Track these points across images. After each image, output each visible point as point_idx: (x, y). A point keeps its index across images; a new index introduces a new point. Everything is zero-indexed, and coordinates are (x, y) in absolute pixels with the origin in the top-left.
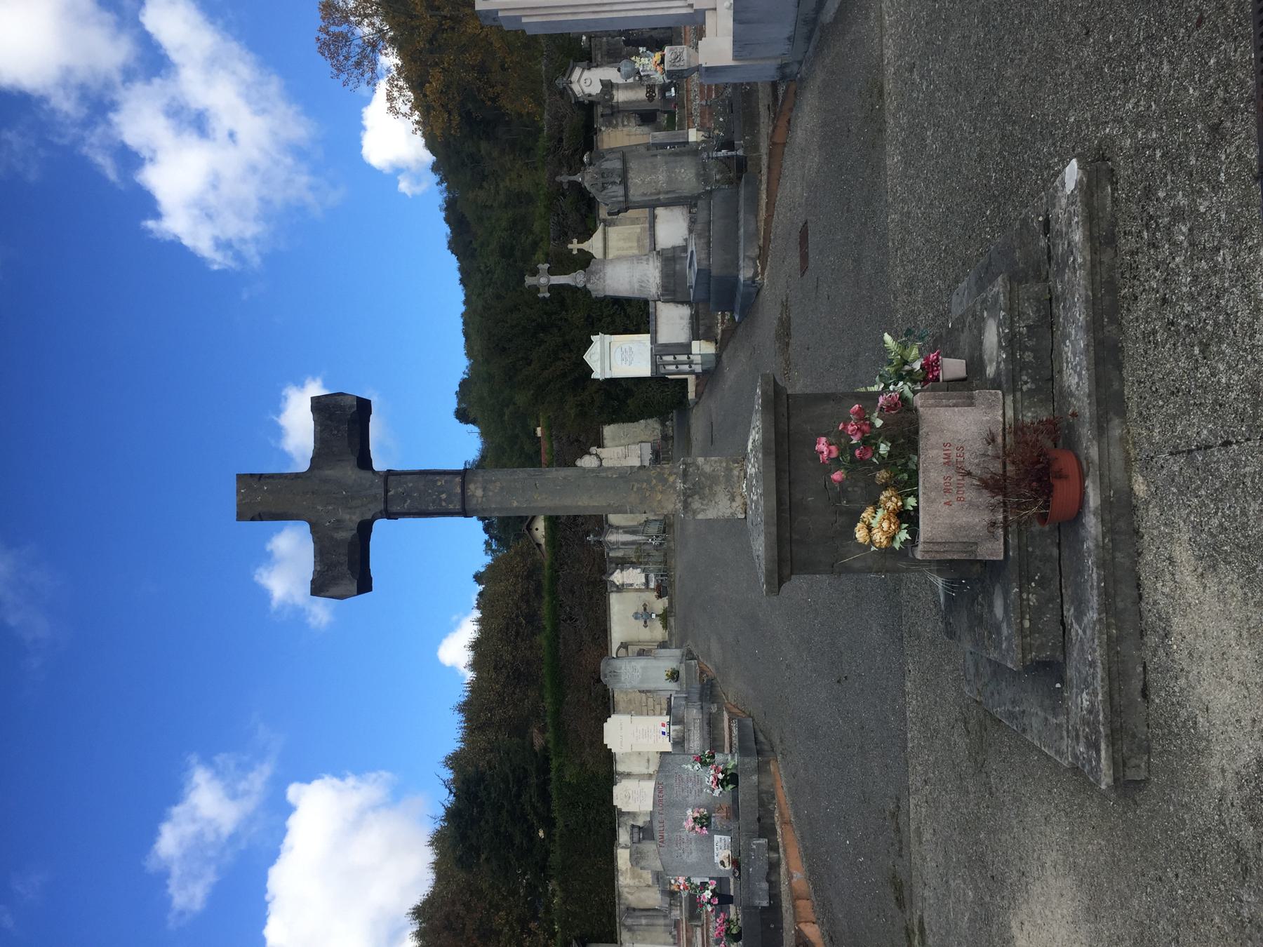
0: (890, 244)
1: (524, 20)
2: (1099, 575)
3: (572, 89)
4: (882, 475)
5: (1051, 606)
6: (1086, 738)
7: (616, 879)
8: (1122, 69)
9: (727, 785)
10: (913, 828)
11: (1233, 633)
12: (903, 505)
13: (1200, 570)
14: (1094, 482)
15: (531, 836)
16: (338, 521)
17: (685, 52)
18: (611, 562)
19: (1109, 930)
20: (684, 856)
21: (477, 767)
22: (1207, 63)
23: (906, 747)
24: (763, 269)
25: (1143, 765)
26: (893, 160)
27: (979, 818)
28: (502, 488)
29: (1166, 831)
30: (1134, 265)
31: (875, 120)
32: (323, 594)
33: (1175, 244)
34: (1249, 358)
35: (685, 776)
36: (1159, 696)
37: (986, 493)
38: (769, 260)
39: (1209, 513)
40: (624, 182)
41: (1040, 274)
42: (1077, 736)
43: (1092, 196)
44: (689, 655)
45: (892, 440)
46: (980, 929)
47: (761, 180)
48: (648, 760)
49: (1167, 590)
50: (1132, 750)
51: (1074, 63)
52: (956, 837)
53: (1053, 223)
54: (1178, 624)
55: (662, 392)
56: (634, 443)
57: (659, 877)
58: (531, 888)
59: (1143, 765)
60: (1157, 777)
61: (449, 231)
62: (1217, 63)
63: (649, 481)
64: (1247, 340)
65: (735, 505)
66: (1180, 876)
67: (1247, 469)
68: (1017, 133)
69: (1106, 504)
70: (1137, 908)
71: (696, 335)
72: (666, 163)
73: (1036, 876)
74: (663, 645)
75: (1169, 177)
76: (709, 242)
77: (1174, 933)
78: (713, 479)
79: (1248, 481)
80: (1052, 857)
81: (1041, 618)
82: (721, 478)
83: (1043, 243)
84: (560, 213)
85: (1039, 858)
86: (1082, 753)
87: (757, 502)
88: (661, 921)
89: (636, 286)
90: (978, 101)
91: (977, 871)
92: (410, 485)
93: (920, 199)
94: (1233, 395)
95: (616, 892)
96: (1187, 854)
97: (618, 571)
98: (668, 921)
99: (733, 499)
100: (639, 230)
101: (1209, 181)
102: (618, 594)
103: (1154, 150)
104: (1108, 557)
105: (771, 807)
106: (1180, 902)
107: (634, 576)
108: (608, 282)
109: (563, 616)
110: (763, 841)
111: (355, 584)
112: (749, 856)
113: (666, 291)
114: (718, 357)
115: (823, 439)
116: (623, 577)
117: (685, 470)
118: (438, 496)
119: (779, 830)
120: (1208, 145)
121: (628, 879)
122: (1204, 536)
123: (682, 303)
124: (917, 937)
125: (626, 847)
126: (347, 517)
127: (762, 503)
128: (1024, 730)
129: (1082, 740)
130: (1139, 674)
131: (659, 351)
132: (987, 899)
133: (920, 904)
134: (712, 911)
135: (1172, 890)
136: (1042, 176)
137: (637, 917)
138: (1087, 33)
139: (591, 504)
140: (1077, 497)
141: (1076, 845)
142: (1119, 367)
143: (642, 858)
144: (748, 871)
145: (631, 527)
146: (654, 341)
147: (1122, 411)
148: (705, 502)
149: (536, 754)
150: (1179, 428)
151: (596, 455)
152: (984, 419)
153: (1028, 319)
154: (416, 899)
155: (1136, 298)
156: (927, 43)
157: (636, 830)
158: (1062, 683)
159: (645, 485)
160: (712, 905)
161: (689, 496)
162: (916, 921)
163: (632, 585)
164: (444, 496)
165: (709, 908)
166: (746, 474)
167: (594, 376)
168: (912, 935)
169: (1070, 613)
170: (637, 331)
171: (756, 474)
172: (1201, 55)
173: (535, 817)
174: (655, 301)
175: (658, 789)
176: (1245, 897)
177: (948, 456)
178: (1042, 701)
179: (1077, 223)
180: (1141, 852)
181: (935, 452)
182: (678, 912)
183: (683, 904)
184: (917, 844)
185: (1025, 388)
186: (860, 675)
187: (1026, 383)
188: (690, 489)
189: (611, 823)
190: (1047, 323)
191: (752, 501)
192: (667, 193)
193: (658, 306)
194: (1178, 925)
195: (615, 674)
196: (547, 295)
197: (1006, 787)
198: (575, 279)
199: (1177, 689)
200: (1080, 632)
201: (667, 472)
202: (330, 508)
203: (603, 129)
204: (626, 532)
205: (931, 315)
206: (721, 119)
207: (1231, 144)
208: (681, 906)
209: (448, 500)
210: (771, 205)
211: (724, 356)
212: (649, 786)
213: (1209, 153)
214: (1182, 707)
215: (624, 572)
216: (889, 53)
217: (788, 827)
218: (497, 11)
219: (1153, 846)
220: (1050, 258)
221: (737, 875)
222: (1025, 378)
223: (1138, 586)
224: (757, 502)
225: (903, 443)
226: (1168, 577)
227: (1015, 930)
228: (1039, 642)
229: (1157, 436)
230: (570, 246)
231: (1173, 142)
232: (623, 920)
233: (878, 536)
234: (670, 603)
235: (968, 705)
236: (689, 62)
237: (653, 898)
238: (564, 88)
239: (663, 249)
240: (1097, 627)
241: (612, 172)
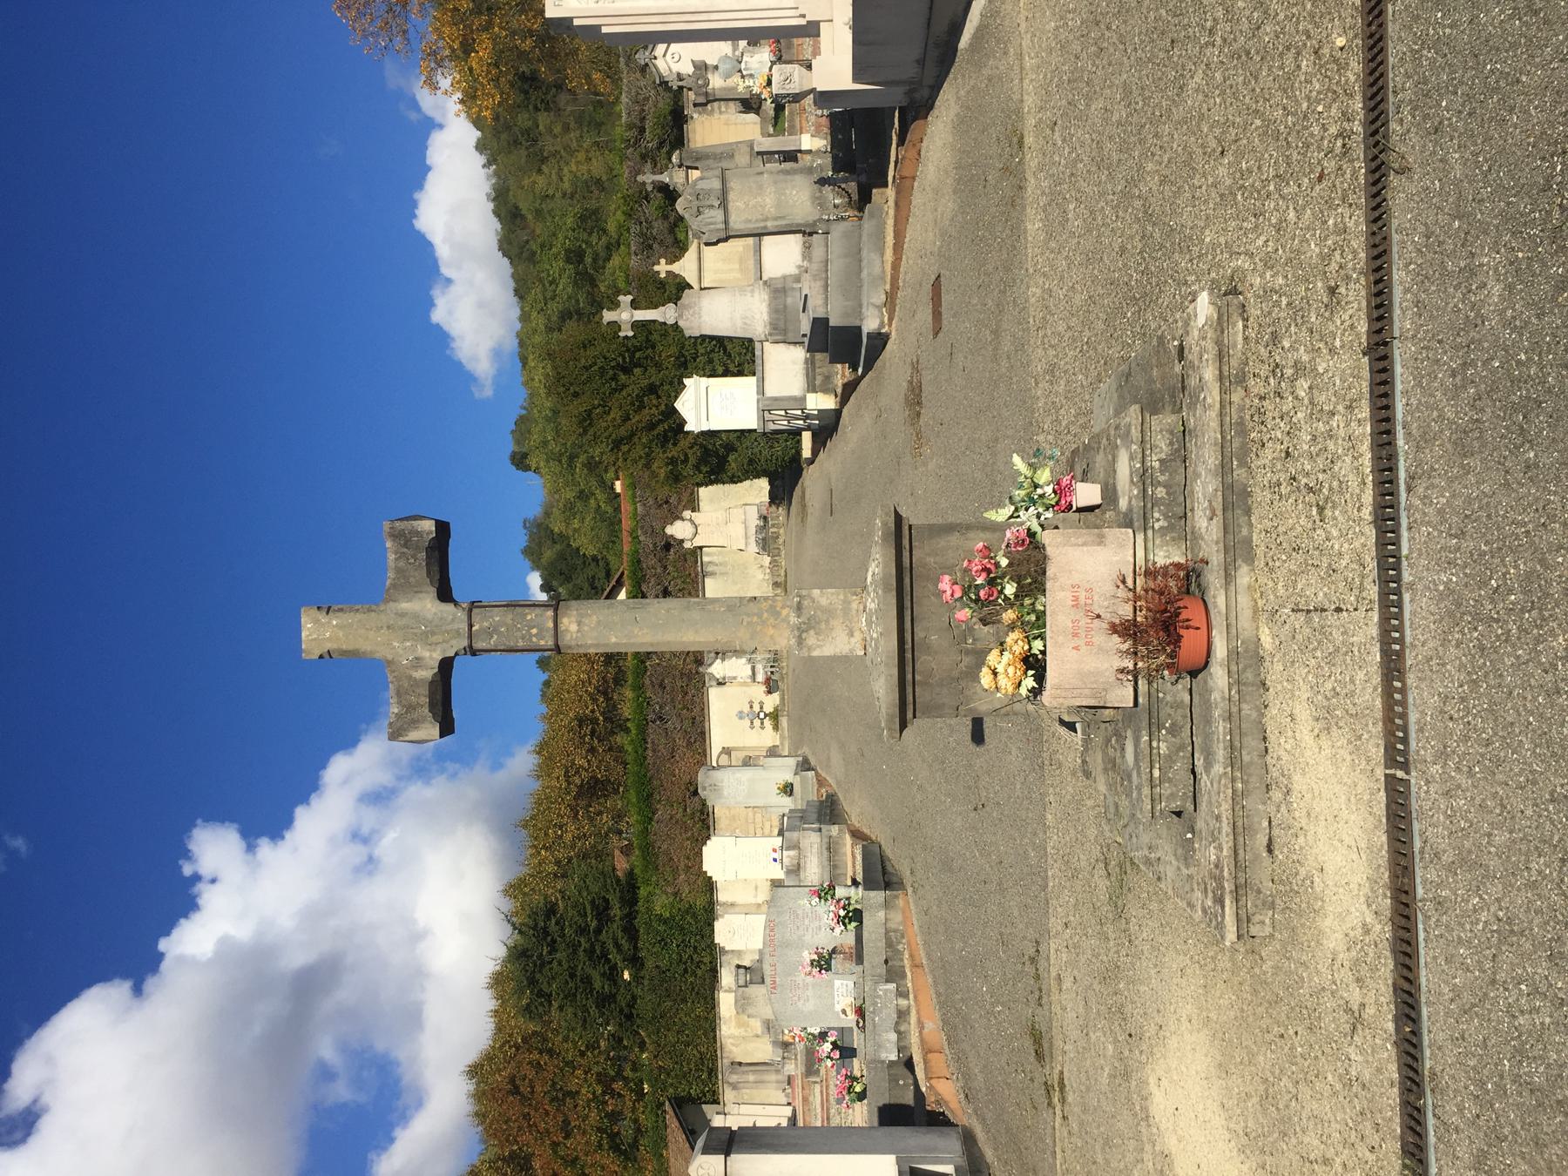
0: (1031, 321)
1: (605, 30)
2: (1225, 728)
3: (655, 66)
4: (1009, 615)
5: (1181, 754)
6: (1213, 892)
7: (718, 1028)
8: (1253, 201)
9: (850, 923)
10: (1053, 974)
11: (1343, 797)
12: (1030, 648)
13: (1316, 731)
14: (1221, 633)
15: (613, 975)
16: (416, 658)
17: (796, 73)
19: (1238, 1087)
20: (800, 1004)
21: (546, 897)
22: (1326, 222)
23: (1047, 886)
24: (891, 320)
25: (1267, 921)
26: (1033, 225)
27: (1118, 967)
28: (599, 622)
29: (1288, 989)
30: (1262, 410)
31: (1013, 173)
32: (401, 738)
33: (1297, 398)
34: (1357, 530)
35: (800, 912)
36: (1281, 853)
37: (1116, 638)
38: (897, 309)
39: (1324, 676)
40: (724, 204)
41: (1176, 402)
42: (1206, 888)
43: (1223, 332)
44: (805, 765)
45: (1018, 579)
46: (1120, 1085)
47: (887, 213)
48: (756, 888)
49: (1288, 747)
50: (1256, 906)
51: (1211, 180)
52: (1096, 987)
53: (1186, 351)
54: (1299, 783)
55: (771, 447)
56: (736, 507)
57: (768, 1026)
58: (617, 1040)
59: (1267, 921)
60: (1281, 934)
61: (499, 226)
62: (1335, 224)
63: (760, 616)
64: (1355, 511)
65: (853, 640)
66: (1299, 1033)
67: (1355, 638)
68: (1157, 235)
69: (1233, 655)
70: (1262, 1064)
72: (775, 183)
73: (1173, 1030)
74: (773, 752)
75: (1292, 328)
76: (826, 286)
77: (1294, 1091)
78: (829, 612)
79: (1355, 650)
80: (1188, 1009)
81: (1171, 767)
83: (1178, 368)
84: (643, 219)
85: (1175, 1012)
86: (1209, 908)
87: (877, 641)
88: (773, 1077)
89: (739, 323)
90: (1120, 188)
91: (1116, 1023)
92: (497, 619)
93: (1062, 278)
94: (1344, 563)
95: (719, 1044)
96: (1304, 1011)
97: (719, 661)
98: (780, 1077)
99: (851, 634)
100: (741, 249)
101: (1326, 343)
103: (1280, 296)
104: (1235, 710)
105: (900, 947)
106: (1299, 1059)
107: (733, 668)
108: (705, 318)
109: (651, 716)
110: (892, 986)
111: (438, 729)
112: (875, 1004)
113: (774, 329)
115: (947, 578)
117: (799, 603)
118: (528, 631)
119: (909, 974)
120: (1326, 306)
121: (732, 1028)
122: (1320, 697)
124: (1057, 1093)
125: (729, 991)
126: (427, 654)
127: (882, 643)
128: (1159, 879)
129: (1210, 895)
130: (1265, 829)
131: (766, 407)
132: (1126, 1053)
133: (1060, 1058)
134: (832, 1067)
135: (1292, 1048)
136: (1180, 291)
137: (743, 1073)
138: (1222, 153)
139: (697, 639)
140: (1205, 655)
141: (1209, 999)
142: (1248, 512)
143: (749, 1004)
144: (873, 1020)
146: (761, 390)
147: (1250, 559)
148: (820, 638)
149: (618, 880)
150: (1299, 587)
151: (691, 520)
152: (1115, 559)
153: (1161, 452)
154: (472, 1056)
155: (1263, 445)
156: (1069, 103)
158: (1193, 832)
159: (755, 619)
160: (832, 1059)
161: (803, 631)
162: (1056, 1077)
163: (735, 678)
164: (534, 631)
165: (829, 1063)
166: (865, 607)
167: (687, 428)
168: (1051, 1092)
169: (1199, 763)
170: (740, 374)
171: (876, 611)
172: (1322, 212)
173: (618, 957)
174: (761, 342)
175: (770, 927)
176: (1353, 1057)
177: (1076, 599)
178: (1176, 850)
179: (1207, 360)
180: (1267, 1008)
181: (1063, 594)
182: (793, 1066)
183: (799, 1057)
184: (1057, 992)
185: (1157, 526)
186: (998, 803)
187: (1158, 520)
188: (805, 623)
189: (711, 962)
190: (1180, 456)
191: (872, 638)
192: (776, 219)
194: (1298, 1082)
195: (715, 787)
196: (631, 334)
197: (1145, 935)
198: (665, 314)
199: (1297, 847)
200: (1208, 783)
202: (408, 644)
203: (695, 116)
205: (1073, 411)
206: (840, 137)
207: (1345, 311)
208: (796, 1059)
209: (540, 635)
210: (898, 247)
211: (845, 411)
212: (759, 921)
213: (1327, 314)
214: (1302, 865)
215: (726, 662)
216: (1030, 101)
217: (919, 971)
218: (571, 19)
219: (1276, 1002)
220: (1183, 388)
221: (861, 1025)
222: (1156, 515)
223: (1265, 739)
224: (877, 641)
225: (1030, 584)
226: (1290, 734)
227: (1153, 1087)
228: (1169, 791)
229: (1281, 591)
230: (656, 268)
231: (1297, 293)
232: (726, 1076)
233: (1005, 683)
234: (782, 699)
235: (1108, 845)
236: (801, 85)
237: (763, 1050)
238: (647, 65)
239: (771, 279)
240: (1223, 782)
241: (709, 192)
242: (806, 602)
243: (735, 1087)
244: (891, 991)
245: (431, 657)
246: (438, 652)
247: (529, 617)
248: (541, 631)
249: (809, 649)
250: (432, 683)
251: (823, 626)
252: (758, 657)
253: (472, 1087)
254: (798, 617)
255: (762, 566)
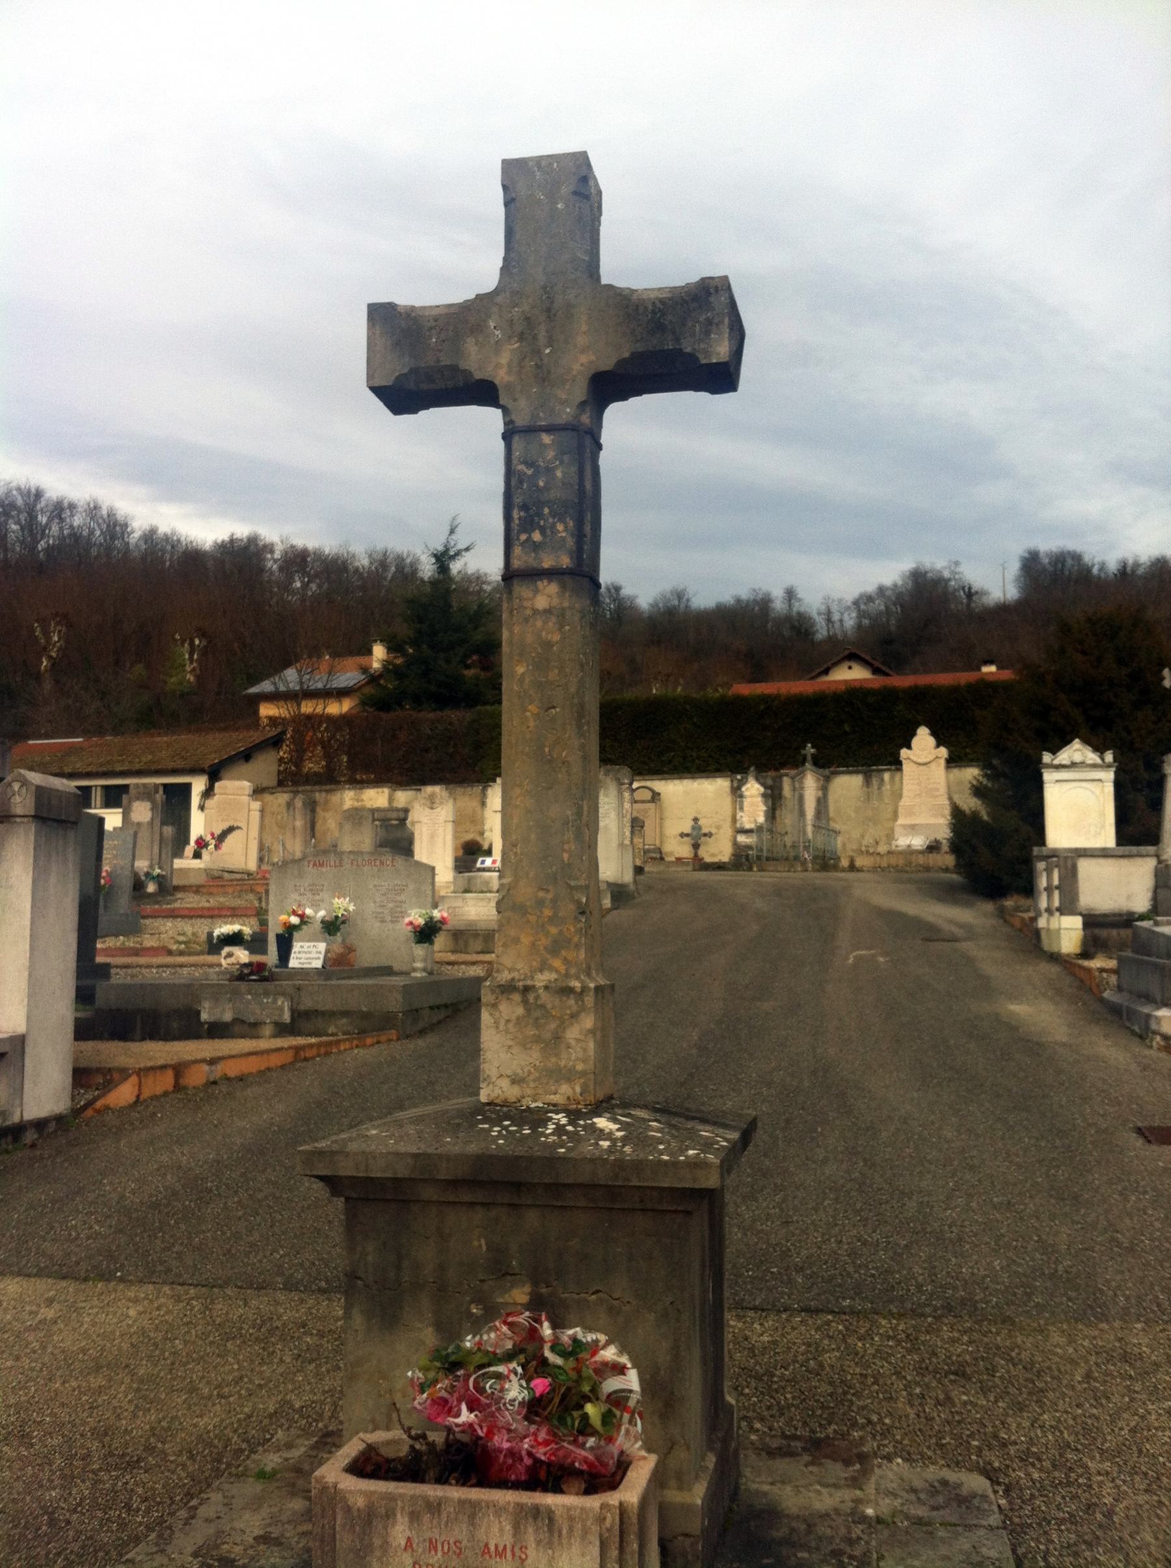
18: (774, 779)
28: (548, 645)
63: (552, 920)
65: (505, 1083)
71: (1092, 922)
82: (553, 1060)
97: (762, 789)
102: (728, 790)
114: (1055, 958)
116: (752, 797)
123: (1155, 899)
125: (391, 800)
131: (1069, 860)
145: (826, 807)
148: (511, 1025)
157: (402, 815)
159: (547, 912)
163: (741, 809)
193: (1148, 859)
201: (571, 955)
204: (819, 801)
215: (760, 799)
242: (572, 1002)
243: (289, 805)
244: (281, 1015)
245: (498, 366)
246: (507, 378)
247: (560, 527)
248: (536, 547)
249: (494, 1006)
250: (454, 369)
251: (531, 1031)
252: (766, 836)
253: (900, 583)
254: (546, 988)
255: (877, 843)
